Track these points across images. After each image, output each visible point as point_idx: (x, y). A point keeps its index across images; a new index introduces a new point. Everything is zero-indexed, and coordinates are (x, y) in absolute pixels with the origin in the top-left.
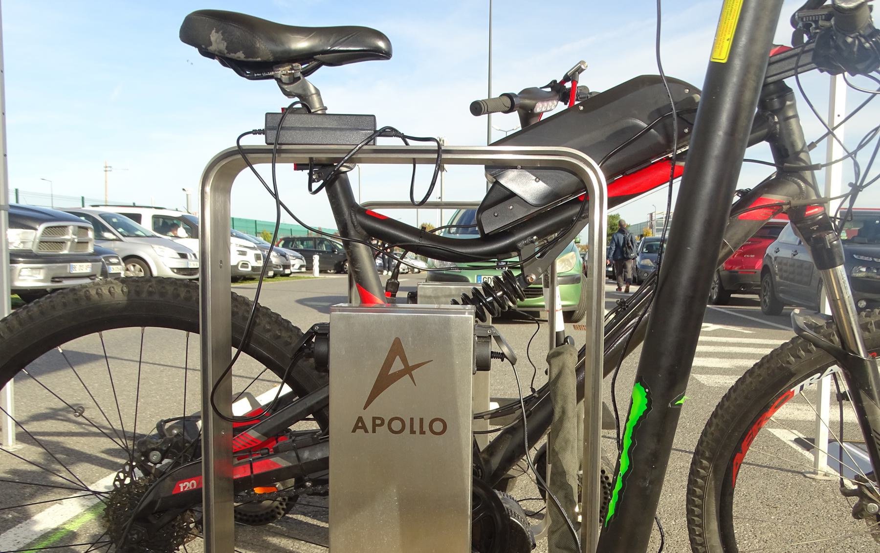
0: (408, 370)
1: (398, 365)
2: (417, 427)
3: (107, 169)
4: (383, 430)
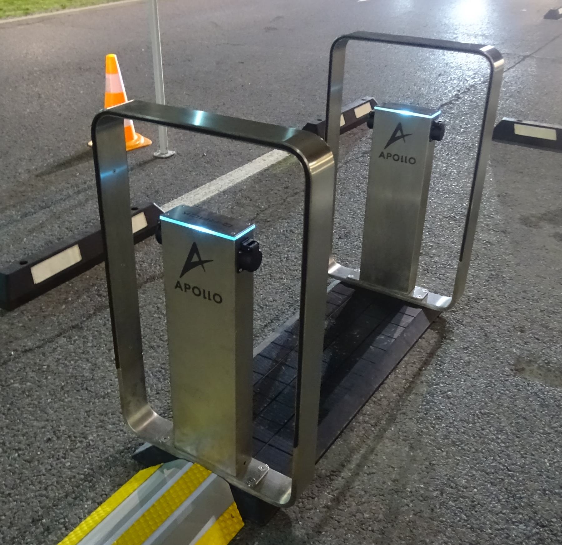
0: (403, 136)
1: (399, 134)
2: (207, 295)
3: (60, 128)
4: (390, 159)
